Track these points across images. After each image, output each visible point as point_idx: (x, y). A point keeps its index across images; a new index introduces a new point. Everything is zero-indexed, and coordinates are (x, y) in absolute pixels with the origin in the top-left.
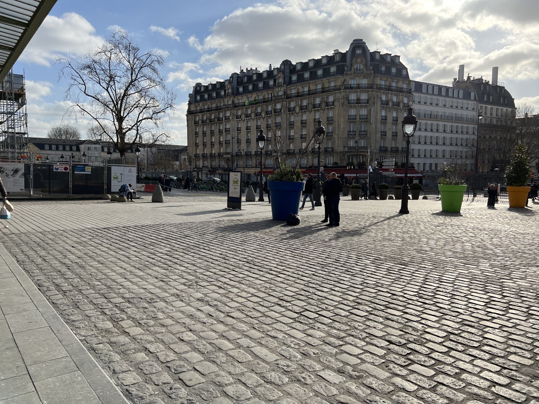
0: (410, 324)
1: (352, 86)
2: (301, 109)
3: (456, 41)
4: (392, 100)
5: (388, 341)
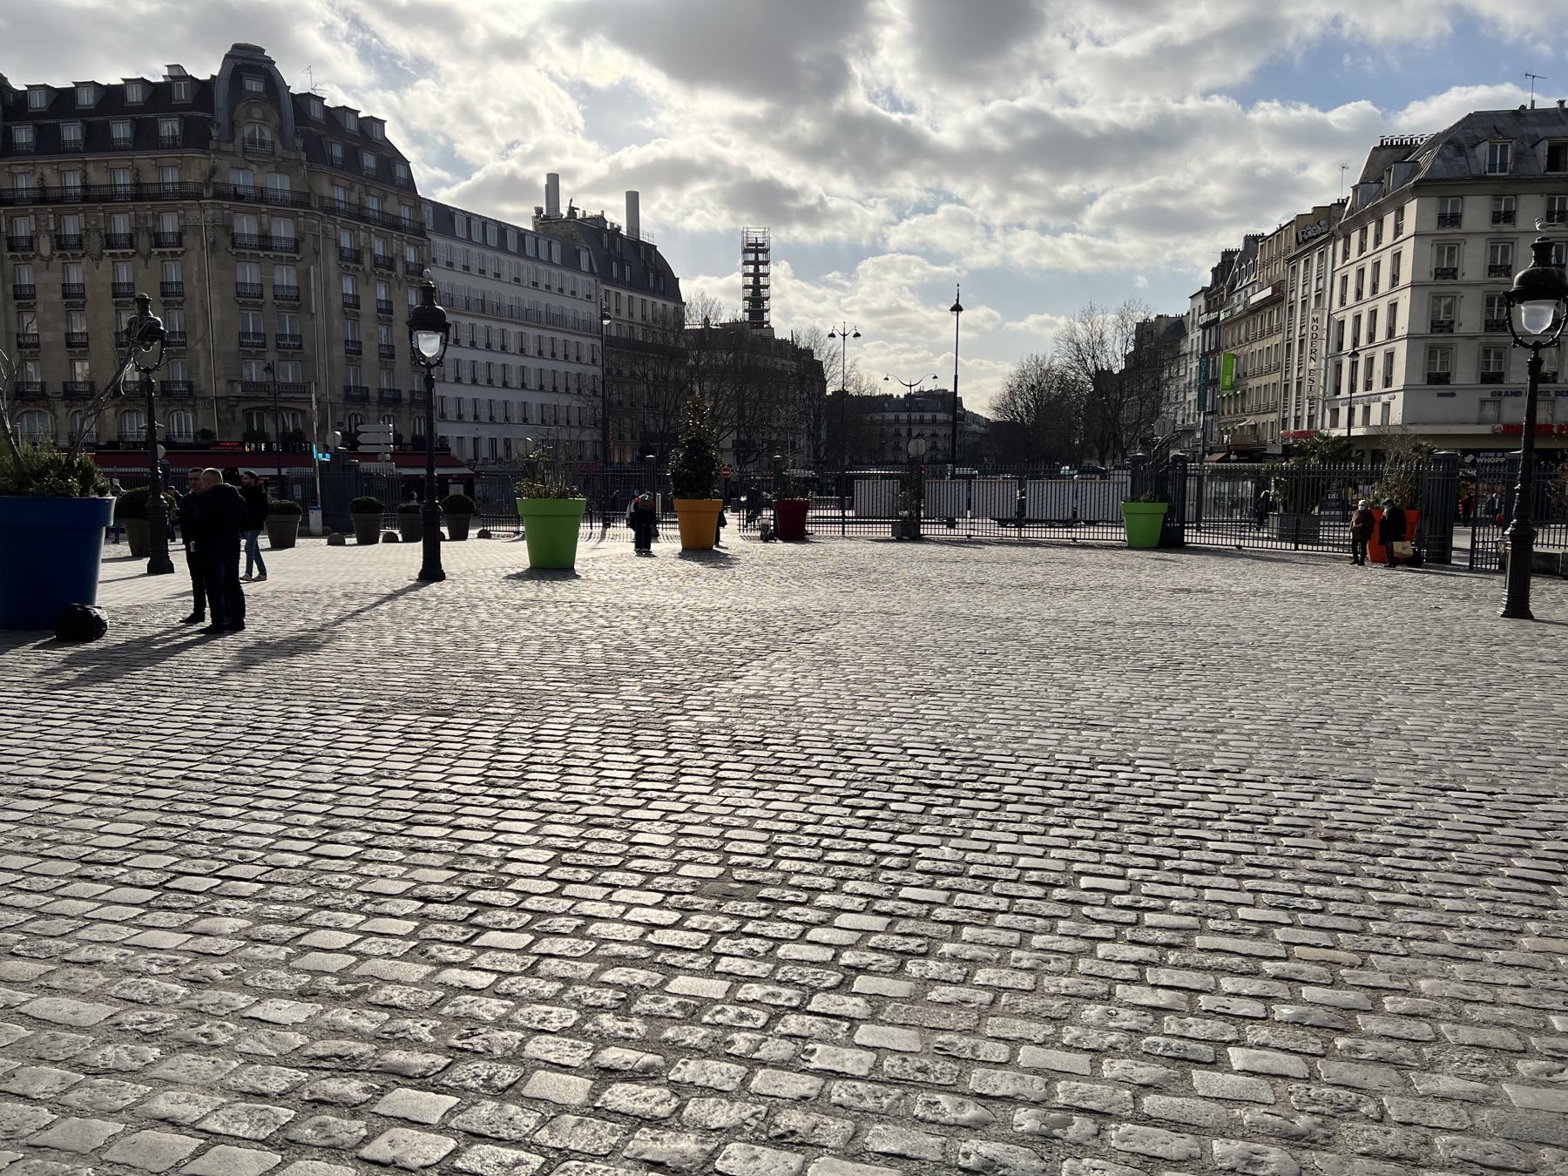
0: (470, 850)
1: (241, 191)
2: (60, 246)
3: (535, 102)
4: (371, 251)
5: (419, 899)
